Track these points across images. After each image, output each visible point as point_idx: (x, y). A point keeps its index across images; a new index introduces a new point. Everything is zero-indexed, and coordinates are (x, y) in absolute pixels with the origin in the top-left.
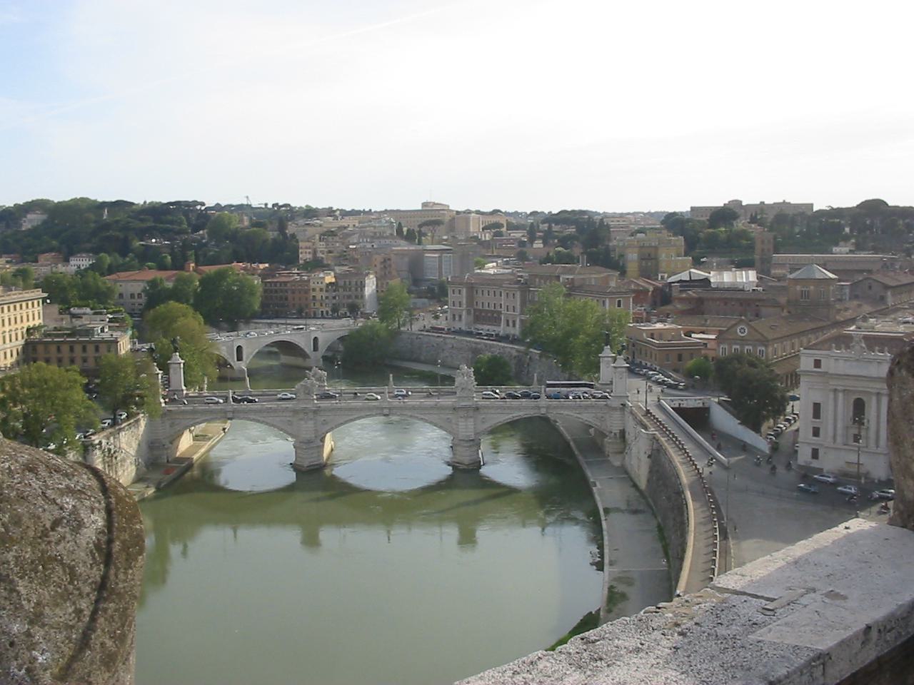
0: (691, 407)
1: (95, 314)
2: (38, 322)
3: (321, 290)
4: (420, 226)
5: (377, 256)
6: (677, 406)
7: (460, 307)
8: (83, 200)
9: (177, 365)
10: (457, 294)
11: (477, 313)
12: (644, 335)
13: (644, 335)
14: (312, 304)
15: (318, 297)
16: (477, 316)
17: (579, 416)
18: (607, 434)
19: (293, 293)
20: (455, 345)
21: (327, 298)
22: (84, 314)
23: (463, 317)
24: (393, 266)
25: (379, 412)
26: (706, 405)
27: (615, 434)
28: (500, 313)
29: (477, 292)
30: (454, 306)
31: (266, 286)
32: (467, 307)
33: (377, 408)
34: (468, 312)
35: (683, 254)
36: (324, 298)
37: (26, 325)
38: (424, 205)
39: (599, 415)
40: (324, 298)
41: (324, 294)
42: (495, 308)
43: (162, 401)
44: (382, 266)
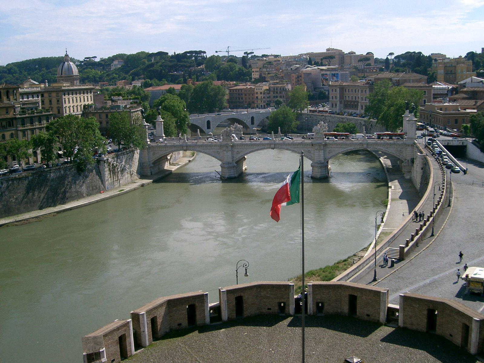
0: (455, 145)
1: (124, 100)
2: (90, 102)
3: (261, 93)
4: (322, 60)
5: (293, 75)
6: (446, 144)
7: (332, 99)
8: (143, 53)
9: (160, 123)
10: (334, 92)
11: (346, 103)
12: (436, 108)
13: (436, 108)
14: (256, 102)
15: (259, 97)
16: (346, 104)
17: (386, 149)
18: (404, 160)
19: (246, 95)
20: (331, 120)
21: (264, 97)
22: (119, 100)
23: (338, 105)
24: (303, 80)
25: (268, 146)
26: (465, 144)
27: (408, 161)
28: (358, 102)
29: (345, 91)
30: (332, 99)
31: (230, 91)
32: (340, 99)
33: (268, 144)
34: (341, 103)
35: (472, 70)
36: (262, 98)
37: (83, 103)
38: (328, 50)
39: (399, 149)
40: (262, 98)
41: (262, 95)
42: (352, 99)
43: (148, 140)
44: (297, 80)
